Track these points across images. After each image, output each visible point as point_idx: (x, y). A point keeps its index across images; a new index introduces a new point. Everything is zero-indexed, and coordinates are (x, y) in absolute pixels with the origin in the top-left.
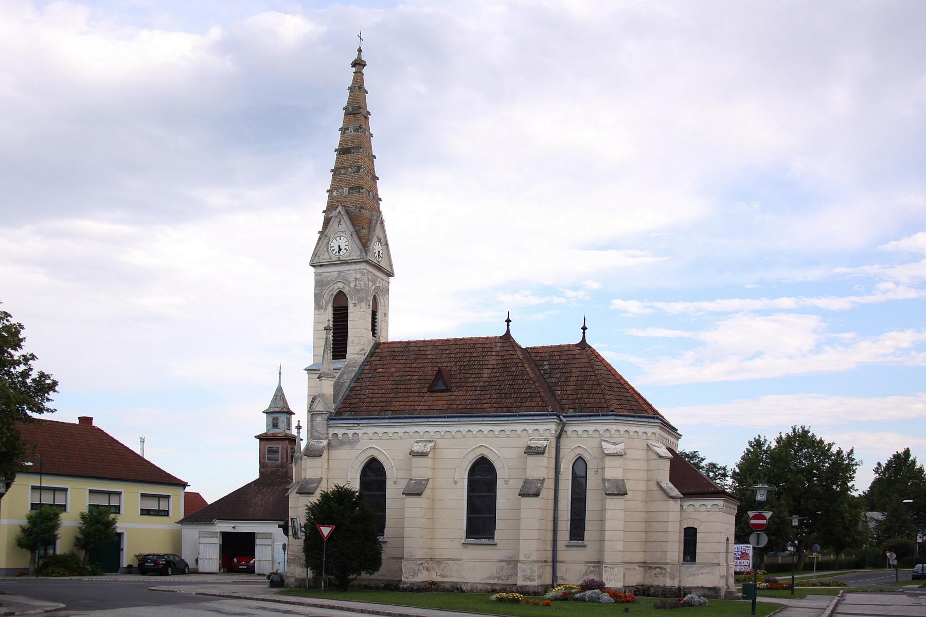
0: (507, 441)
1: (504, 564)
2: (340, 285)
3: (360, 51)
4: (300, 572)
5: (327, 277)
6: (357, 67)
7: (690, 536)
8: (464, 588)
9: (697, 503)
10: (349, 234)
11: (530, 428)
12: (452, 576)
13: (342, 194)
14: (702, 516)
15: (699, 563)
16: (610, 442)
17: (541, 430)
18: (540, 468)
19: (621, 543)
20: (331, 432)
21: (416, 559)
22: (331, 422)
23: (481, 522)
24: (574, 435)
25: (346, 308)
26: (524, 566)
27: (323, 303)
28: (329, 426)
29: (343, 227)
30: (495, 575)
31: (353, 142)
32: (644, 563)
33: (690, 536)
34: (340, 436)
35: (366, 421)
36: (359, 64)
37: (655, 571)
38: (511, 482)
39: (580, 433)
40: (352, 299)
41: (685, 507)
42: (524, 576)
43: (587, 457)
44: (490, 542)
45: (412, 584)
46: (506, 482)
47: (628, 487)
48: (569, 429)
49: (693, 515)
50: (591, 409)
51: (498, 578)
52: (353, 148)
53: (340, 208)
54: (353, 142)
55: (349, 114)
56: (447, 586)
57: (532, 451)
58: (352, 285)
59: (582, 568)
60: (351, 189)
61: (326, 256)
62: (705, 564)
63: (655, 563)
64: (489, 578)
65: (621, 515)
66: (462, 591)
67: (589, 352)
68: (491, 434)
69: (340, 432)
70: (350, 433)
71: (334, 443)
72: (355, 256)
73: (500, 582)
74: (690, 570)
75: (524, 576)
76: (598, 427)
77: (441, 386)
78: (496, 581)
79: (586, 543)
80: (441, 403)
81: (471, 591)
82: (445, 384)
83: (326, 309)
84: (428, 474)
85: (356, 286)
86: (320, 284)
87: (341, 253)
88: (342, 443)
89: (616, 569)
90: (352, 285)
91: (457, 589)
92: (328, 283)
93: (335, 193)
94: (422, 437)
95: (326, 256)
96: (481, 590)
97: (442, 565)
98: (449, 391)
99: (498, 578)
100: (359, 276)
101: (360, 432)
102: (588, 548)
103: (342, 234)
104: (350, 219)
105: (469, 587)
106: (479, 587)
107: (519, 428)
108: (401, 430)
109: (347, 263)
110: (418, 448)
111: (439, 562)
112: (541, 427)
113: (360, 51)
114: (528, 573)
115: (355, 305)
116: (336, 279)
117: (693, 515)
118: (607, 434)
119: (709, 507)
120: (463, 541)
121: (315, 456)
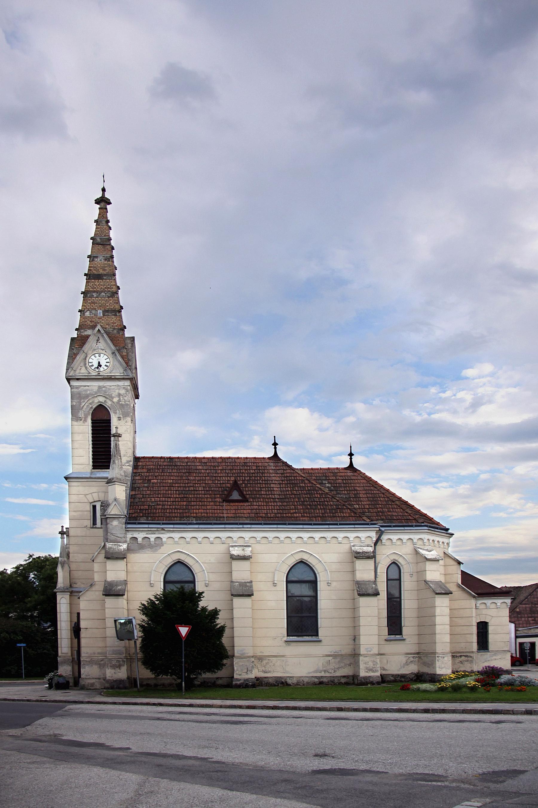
0: (327, 548)
1: (330, 658)
2: (102, 399)
3: (104, 190)
4: (144, 673)
5: (86, 390)
6: (103, 204)
7: (483, 628)
8: (289, 681)
9: (489, 601)
10: (110, 353)
11: (352, 535)
12: (276, 671)
13: (96, 315)
14: (492, 612)
15: (497, 652)
16: (424, 550)
17: (362, 537)
18: (364, 571)
19: (448, 636)
20: (129, 535)
21: (249, 657)
22: (129, 526)
23: (302, 619)
24: (388, 543)
25: (109, 421)
26: (367, 659)
27: (81, 414)
28: (127, 530)
29: (102, 344)
30: (321, 668)
31: (104, 270)
32: (418, 653)
33: (483, 628)
34: (140, 540)
35: (172, 526)
36: (103, 202)
37: (460, 659)
38: (334, 584)
39: (294, 539)
40: (115, 413)
41: (478, 605)
42: (367, 668)
43: (401, 561)
44: (314, 638)
45: (247, 680)
46: (329, 584)
47: (255, 588)
48: (385, 537)
49: (484, 612)
50: (400, 520)
51: (325, 671)
52: (105, 275)
53: (99, 327)
54: (104, 270)
55: (98, 244)
56: (271, 680)
57: (359, 556)
58: (115, 400)
59: (403, 659)
60: (105, 312)
61: (83, 371)
62: (497, 651)
63: (459, 653)
64: (314, 672)
65: (447, 611)
66: (288, 685)
67: (359, 473)
68: (311, 540)
69: (140, 536)
70: (152, 537)
71: (134, 546)
72: (118, 372)
73: (327, 675)
74: (485, 657)
75: (367, 668)
76: (411, 536)
77: (235, 495)
78: (323, 674)
79: (404, 637)
80: (245, 511)
81: (298, 684)
82: (241, 493)
83: (85, 420)
84: (121, 576)
85: (119, 401)
86: (77, 397)
87: (101, 369)
88: (142, 547)
89: (446, 658)
90: (115, 400)
91: (282, 683)
92: (87, 396)
93: (87, 314)
94: (236, 542)
95: (83, 371)
96: (308, 683)
97: (264, 662)
98: (247, 501)
99: (325, 671)
100: (122, 392)
101: (164, 536)
102: (407, 641)
103: (101, 351)
104: (112, 340)
105: (295, 681)
106: (306, 680)
107: (340, 535)
108: (212, 535)
109: (110, 378)
110: (236, 552)
111: (260, 659)
112: (363, 535)
113: (104, 190)
114: (371, 665)
115: (119, 419)
116: (96, 393)
117: (484, 612)
118: (420, 542)
119: (499, 604)
120: (286, 638)
121: (117, 558)
